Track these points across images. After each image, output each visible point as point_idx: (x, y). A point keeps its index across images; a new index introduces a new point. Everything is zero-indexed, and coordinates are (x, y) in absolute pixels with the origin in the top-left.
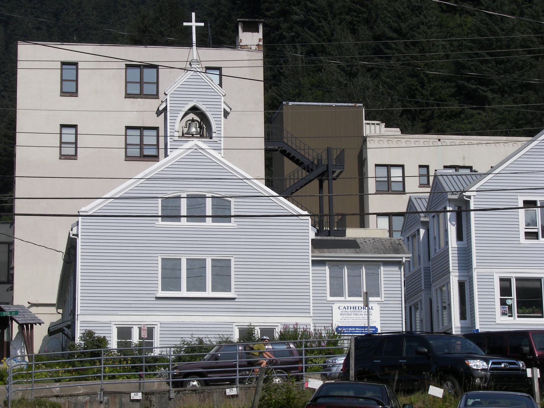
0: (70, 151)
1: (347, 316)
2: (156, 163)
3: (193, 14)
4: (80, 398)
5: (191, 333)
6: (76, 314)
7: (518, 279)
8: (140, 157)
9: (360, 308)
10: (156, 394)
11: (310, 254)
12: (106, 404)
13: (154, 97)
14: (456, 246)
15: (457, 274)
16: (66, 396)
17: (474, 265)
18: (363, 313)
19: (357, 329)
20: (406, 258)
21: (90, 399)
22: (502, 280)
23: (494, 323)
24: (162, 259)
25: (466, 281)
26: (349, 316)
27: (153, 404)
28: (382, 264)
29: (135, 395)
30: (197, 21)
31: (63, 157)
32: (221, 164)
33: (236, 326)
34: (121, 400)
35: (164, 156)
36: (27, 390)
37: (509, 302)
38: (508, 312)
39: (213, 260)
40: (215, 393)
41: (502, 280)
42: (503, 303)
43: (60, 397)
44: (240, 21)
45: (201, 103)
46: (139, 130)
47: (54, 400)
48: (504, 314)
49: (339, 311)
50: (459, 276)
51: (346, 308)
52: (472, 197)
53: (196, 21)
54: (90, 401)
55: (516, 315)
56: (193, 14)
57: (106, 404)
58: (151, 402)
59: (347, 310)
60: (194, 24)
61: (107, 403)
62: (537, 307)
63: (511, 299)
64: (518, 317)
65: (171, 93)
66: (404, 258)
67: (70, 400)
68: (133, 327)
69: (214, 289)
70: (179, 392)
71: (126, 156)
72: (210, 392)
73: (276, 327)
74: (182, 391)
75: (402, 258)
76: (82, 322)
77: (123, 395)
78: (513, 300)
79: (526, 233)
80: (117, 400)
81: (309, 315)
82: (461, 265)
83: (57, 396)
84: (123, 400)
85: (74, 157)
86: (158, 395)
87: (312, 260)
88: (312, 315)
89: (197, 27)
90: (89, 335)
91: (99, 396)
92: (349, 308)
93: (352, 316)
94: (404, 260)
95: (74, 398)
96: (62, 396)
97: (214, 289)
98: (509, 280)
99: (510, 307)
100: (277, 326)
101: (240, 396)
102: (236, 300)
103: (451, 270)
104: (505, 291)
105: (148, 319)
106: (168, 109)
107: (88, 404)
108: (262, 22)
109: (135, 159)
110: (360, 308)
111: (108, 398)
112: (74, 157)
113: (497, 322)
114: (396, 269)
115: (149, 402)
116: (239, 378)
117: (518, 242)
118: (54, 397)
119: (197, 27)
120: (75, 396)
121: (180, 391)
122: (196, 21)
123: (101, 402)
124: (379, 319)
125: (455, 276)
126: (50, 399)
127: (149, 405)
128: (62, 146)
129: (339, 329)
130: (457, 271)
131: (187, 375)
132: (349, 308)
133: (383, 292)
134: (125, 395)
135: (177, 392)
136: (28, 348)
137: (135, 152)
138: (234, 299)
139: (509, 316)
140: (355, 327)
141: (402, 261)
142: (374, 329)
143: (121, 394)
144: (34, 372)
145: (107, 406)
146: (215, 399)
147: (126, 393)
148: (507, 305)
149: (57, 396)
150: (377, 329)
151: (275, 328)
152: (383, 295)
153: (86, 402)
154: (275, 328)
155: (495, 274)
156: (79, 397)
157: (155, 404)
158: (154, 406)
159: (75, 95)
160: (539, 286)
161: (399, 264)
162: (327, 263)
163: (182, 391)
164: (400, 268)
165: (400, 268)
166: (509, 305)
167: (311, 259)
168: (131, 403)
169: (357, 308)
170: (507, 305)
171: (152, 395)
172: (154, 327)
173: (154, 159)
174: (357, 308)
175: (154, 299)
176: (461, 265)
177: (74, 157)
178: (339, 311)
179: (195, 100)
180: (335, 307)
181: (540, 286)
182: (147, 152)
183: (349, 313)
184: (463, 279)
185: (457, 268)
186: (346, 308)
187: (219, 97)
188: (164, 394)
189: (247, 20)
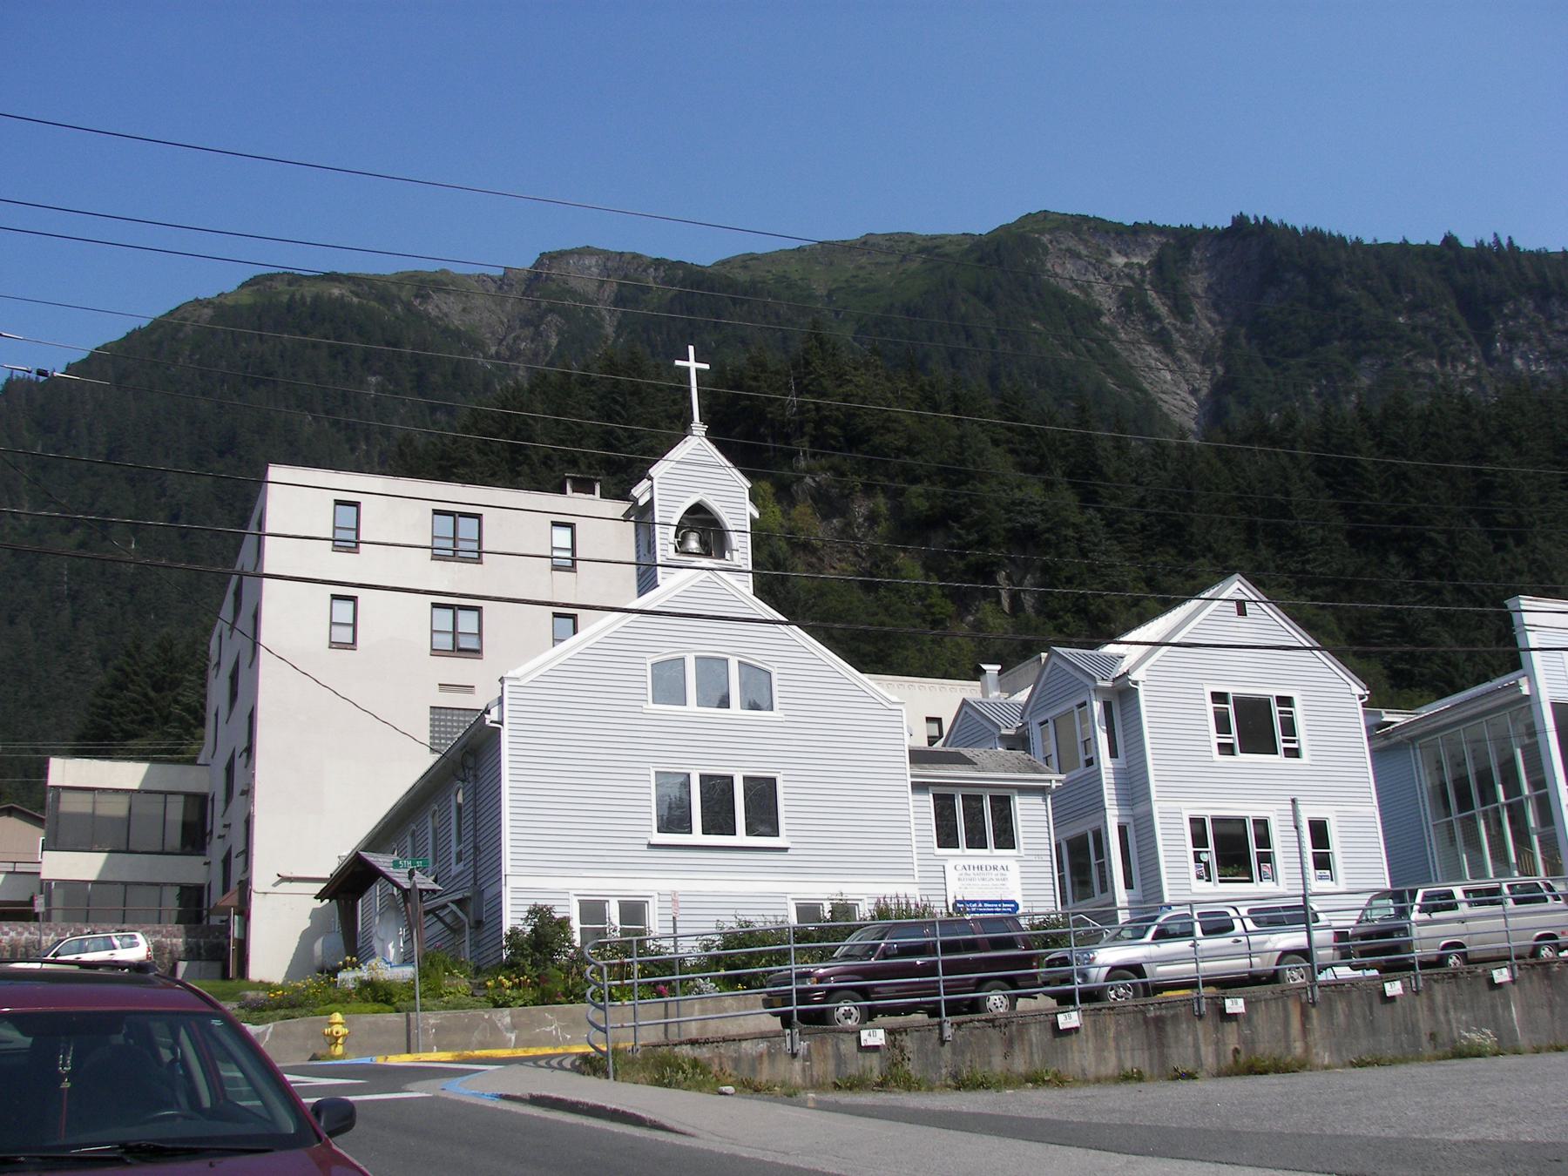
0: (344, 635)
1: (968, 882)
3: (691, 348)
4: (746, 1046)
5: (733, 912)
6: (503, 873)
7: (1215, 820)
10: (911, 1031)
12: (805, 1060)
15: (1117, 812)
16: (712, 1043)
17: (1154, 796)
18: (994, 877)
19: (986, 905)
20: (1057, 781)
21: (769, 1047)
22: (1192, 820)
24: (656, 772)
27: (908, 1055)
28: (1015, 791)
29: (870, 1035)
34: (838, 1049)
36: (622, 1027)
37: (1204, 857)
40: (1033, 1026)
41: (1192, 820)
42: (1197, 859)
43: (699, 1043)
44: (568, 477)
45: (711, 498)
47: (687, 1049)
48: (1199, 877)
49: (956, 874)
50: (1120, 816)
52: (1140, 683)
53: (688, 369)
54: (770, 1054)
55: (1218, 878)
57: (805, 1060)
58: (902, 1051)
59: (968, 872)
60: (693, 365)
61: (808, 1057)
64: (1221, 881)
65: (659, 475)
67: (722, 1051)
69: (750, 831)
70: (959, 1025)
72: (1023, 1024)
73: (859, 902)
74: (966, 1022)
75: (1051, 781)
76: (515, 890)
77: (841, 1036)
78: (1210, 855)
79: (1219, 744)
80: (829, 1049)
81: (912, 881)
83: (693, 1042)
84: (842, 1047)
85: (352, 645)
86: (916, 1033)
87: (913, 783)
88: (917, 880)
90: (540, 914)
91: (788, 1039)
93: (977, 882)
94: (1054, 785)
95: (733, 1046)
96: (706, 1042)
97: (750, 831)
99: (1207, 865)
101: (1082, 1031)
102: (790, 852)
103: (1107, 806)
104: (1199, 840)
107: (765, 1058)
108: (599, 481)
109: (446, 653)
111: (809, 1045)
112: (352, 647)
113: (1194, 890)
114: (1038, 800)
115: (897, 1052)
117: (1210, 759)
118: (686, 1044)
119: (697, 370)
120: (734, 1040)
121: (963, 1023)
122: (688, 369)
123: (794, 1055)
125: (1114, 816)
126: (677, 1049)
127: (900, 1059)
131: (980, 984)
134: (846, 1035)
135: (955, 1026)
136: (40, 987)
137: (446, 642)
138: (786, 849)
140: (983, 902)
141: (1050, 786)
143: (837, 1035)
145: (808, 1063)
146: (1034, 1040)
147: (848, 1032)
149: (693, 1042)
150: (1017, 906)
152: (1022, 846)
153: (761, 1055)
156: (744, 1044)
157: (911, 1056)
158: (909, 1059)
160: (1241, 831)
161: (1041, 791)
162: (931, 789)
163: (966, 1022)
165: (1045, 800)
167: (910, 780)
168: (859, 1055)
171: (904, 1034)
175: (645, 848)
177: (352, 645)
178: (956, 874)
180: (949, 866)
182: (464, 643)
183: (972, 876)
184: (1125, 820)
187: (742, 490)
188: (929, 1030)
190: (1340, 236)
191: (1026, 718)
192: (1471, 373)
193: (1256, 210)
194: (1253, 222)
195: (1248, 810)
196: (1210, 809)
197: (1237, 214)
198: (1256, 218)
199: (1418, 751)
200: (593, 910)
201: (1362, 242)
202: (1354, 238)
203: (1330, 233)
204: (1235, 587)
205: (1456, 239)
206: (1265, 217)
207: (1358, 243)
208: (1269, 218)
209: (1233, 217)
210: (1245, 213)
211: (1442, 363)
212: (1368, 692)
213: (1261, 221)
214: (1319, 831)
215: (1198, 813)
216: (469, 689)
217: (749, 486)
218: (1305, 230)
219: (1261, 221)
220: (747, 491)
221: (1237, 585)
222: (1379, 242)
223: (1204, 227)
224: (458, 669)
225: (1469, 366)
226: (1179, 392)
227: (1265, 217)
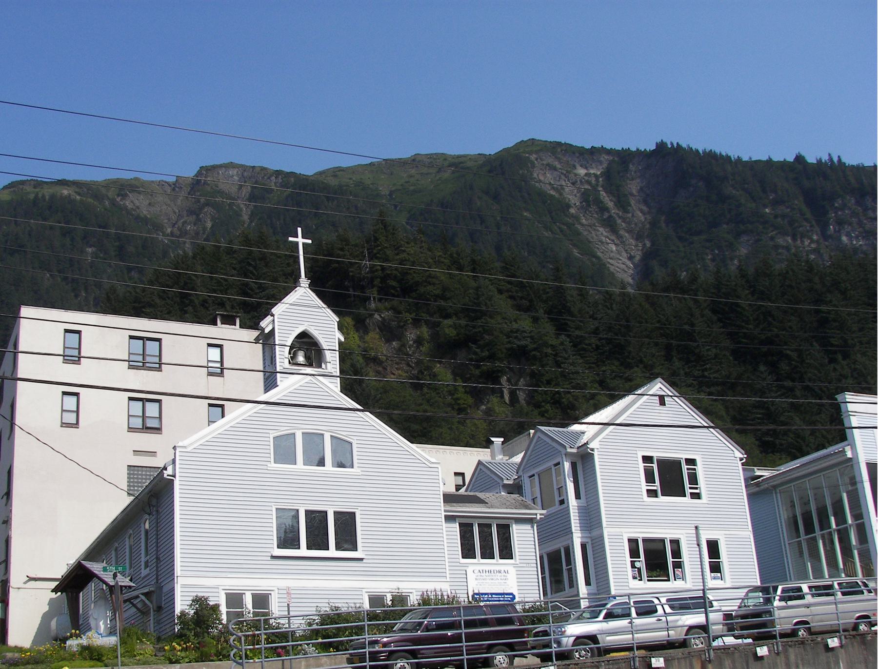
0: (71, 418)
2: (244, 405)
3: (299, 230)
7: (645, 541)
8: (143, 429)
9: (495, 572)
11: (443, 509)
13: (158, 369)
14: (577, 505)
15: (580, 535)
18: (499, 578)
19: (494, 596)
20: (540, 514)
22: (510, 557)
23: (627, 588)
24: (277, 509)
25: (587, 542)
26: (485, 581)
30: (297, 243)
31: (64, 425)
32: (340, 399)
33: (366, 592)
35: (262, 389)
37: (637, 565)
38: (638, 576)
39: (335, 513)
41: (630, 540)
42: (633, 566)
44: (218, 314)
45: (313, 328)
46: (142, 402)
48: (634, 578)
49: (474, 576)
50: (582, 537)
51: (481, 572)
52: (596, 450)
53: (297, 243)
56: (299, 230)
59: (482, 574)
60: (300, 240)
62: (661, 570)
63: (639, 561)
66: (538, 515)
68: (245, 594)
69: (338, 547)
71: (129, 428)
75: (536, 514)
78: (641, 563)
79: (648, 490)
81: (446, 580)
82: (582, 525)
85: (76, 425)
88: (448, 579)
89: (304, 244)
92: (484, 571)
93: (488, 581)
94: (539, 517)
97: (338, 547)
98: (502, 557)
100: (411, 593)
102: (364, 561)
103: (573, 531)
104: (634, 553)
105: (262, 584)
106: (277, 335)
108: (239, 317)
110: (495, 572)
116: (467, 659)
119: (304, 244)
124: (516, 584)
125: (578, 537)
128: (158, 365)
129: (475, 596)
130: (579, 532)
132: (484, 571)
133: (517, 554)
138: (362, 559)
139: (639, 580)
140: (492, 594)
142: (511, 596)
144: (777, 643)
148: (636, 568)
151: (409, 596)
154: (409, 596)
155: (624, 534)
159: (78, 363)
160: (662, 548)
161: (530, 521)
162: (457, 520)
164: (533, 527)
165: (533, 527)
166: (638, 568)
167: (444, 514)
169: (492, 572)
170: (636, 568)
172: (270, 594)
173: (158, 432)
174: (492, 572)
175: (269, 558)
176: (582, 525)
177: (76, 425)
178: (474, 576)
179: (306, 324)
181: (662, 548)
183: (485, 577)
184: (585, 540)
185: (579, 528)
186: (481, 572)
189: (225, 313)
190: (727, 155)
191: (520, 473)
192: (813, 246)
193: (672, 138)
194: (670, 146)
195: (667, 534)
196: (641, 533)
197: (659, 141)
198: (672, 144)
199: (779, 495)
200: (234, 599)
201: (741, 160)
202: (736, 157)
203: (720, 154)
204: (658, 387)
205: (803, 157)
206: (678, 143)
207: (739, 160)
208: (680, 143)
209: (657, 143)
210: (664, 141)
211: (794, 239)
212: (745, 456)
213: (675, 145)
214: (713, 548)
215: (634, 536)
216: (153, 453)
217: (338, 320)
218: (704, 152)
219: (675, 145)
220: (336, 324)
221: (659, 385)
222: (753, 159)
223: (638, 149)
224: (146, 441)
225: (812, 241)
226: (621, 258)
227: (678, 143)
